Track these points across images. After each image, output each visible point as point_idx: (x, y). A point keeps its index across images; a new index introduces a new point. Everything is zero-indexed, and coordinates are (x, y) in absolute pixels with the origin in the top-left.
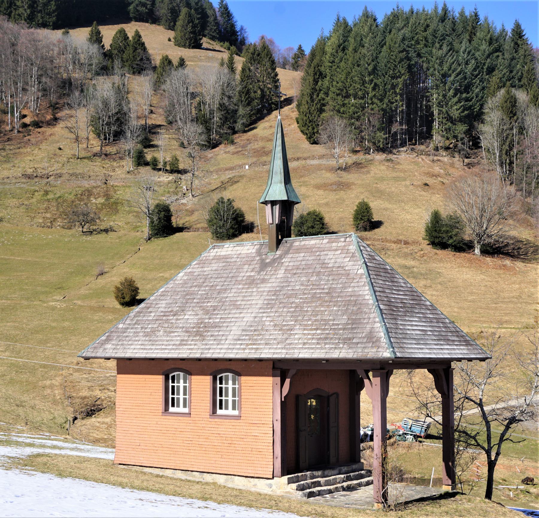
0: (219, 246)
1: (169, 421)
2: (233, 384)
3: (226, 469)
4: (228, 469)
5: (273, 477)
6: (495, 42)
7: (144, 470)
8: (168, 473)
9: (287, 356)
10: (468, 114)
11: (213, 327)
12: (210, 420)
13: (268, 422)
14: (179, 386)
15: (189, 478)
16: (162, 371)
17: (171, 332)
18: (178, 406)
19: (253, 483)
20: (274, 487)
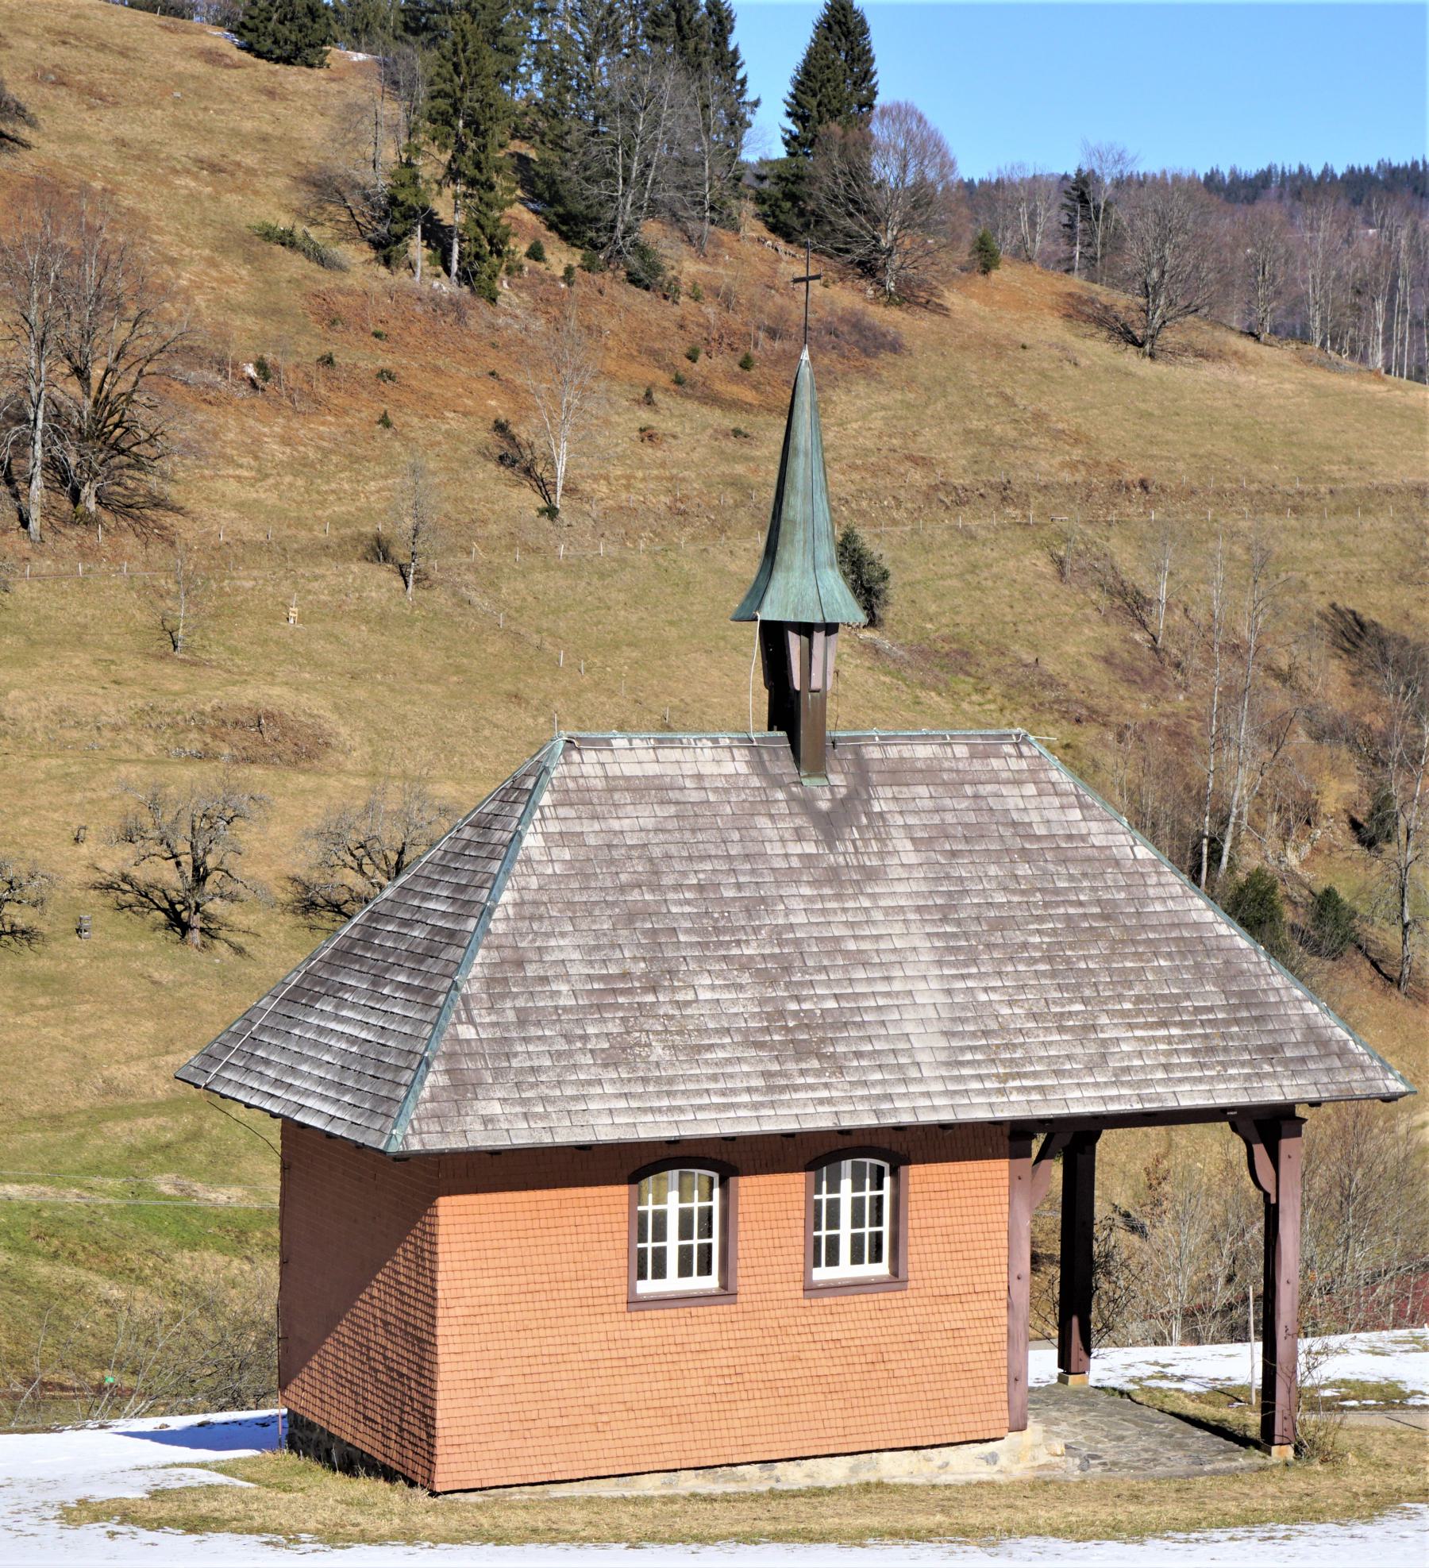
0: (672, 740)
1: (650, 1327)
2: (855, 1189)
3: (861, 1437)
4: (868, 1437)
5: (1266, 1439)
6: (1293, 178)
7: (554, 1495)
8: (649, 1485)
9: (1147, 1105)
10: (364, 63)
11: (834, 1026)
12: (807, 1303)
13: (994, 1287)
14: (854, 1226)
15: (731, 1488)
16: (626, 1172)
17: (699, 1049)
18: (660, 1272)
19: (938, 1462)
20: (1003, 1461)
